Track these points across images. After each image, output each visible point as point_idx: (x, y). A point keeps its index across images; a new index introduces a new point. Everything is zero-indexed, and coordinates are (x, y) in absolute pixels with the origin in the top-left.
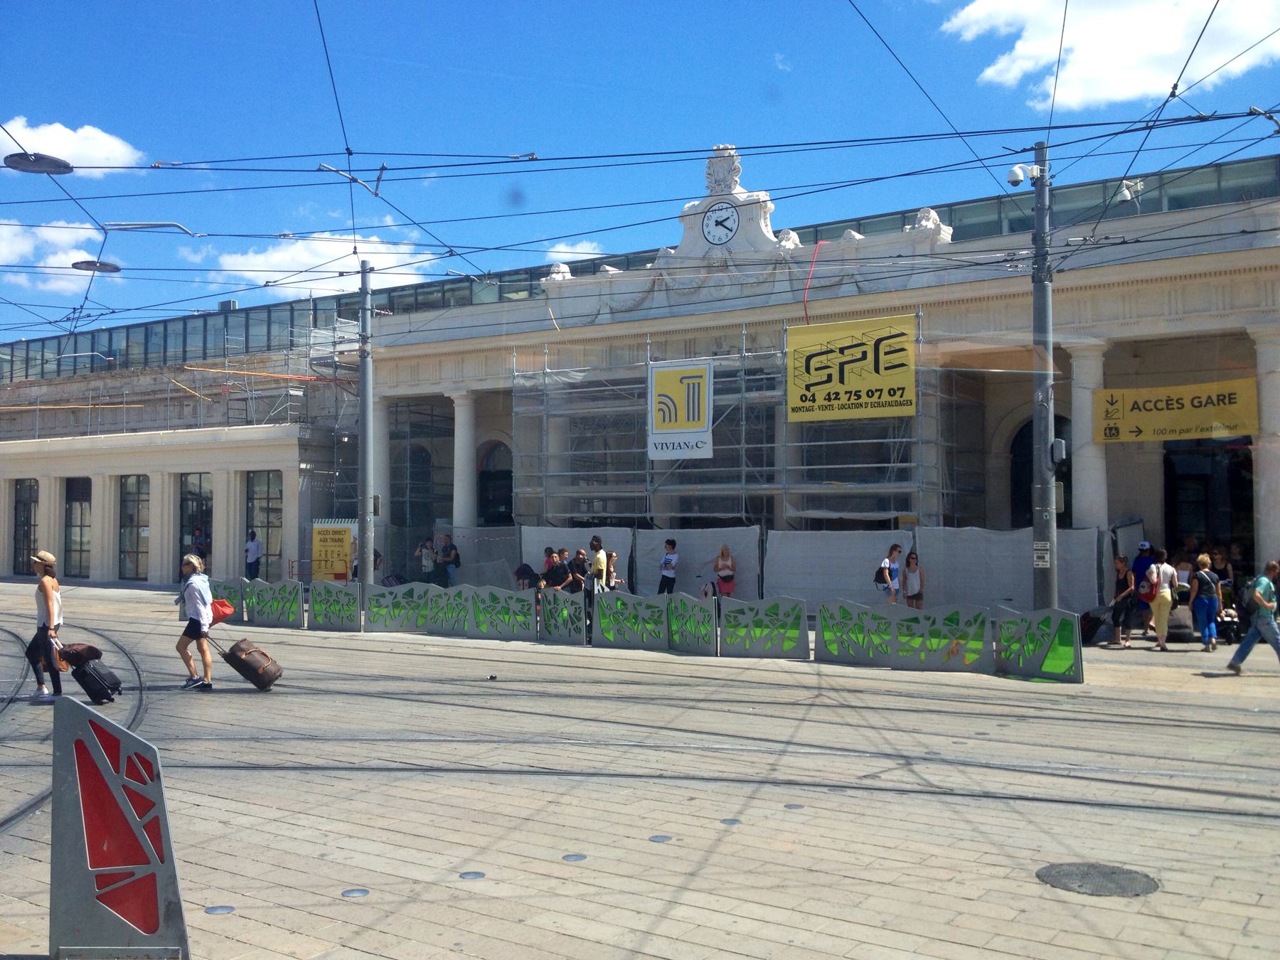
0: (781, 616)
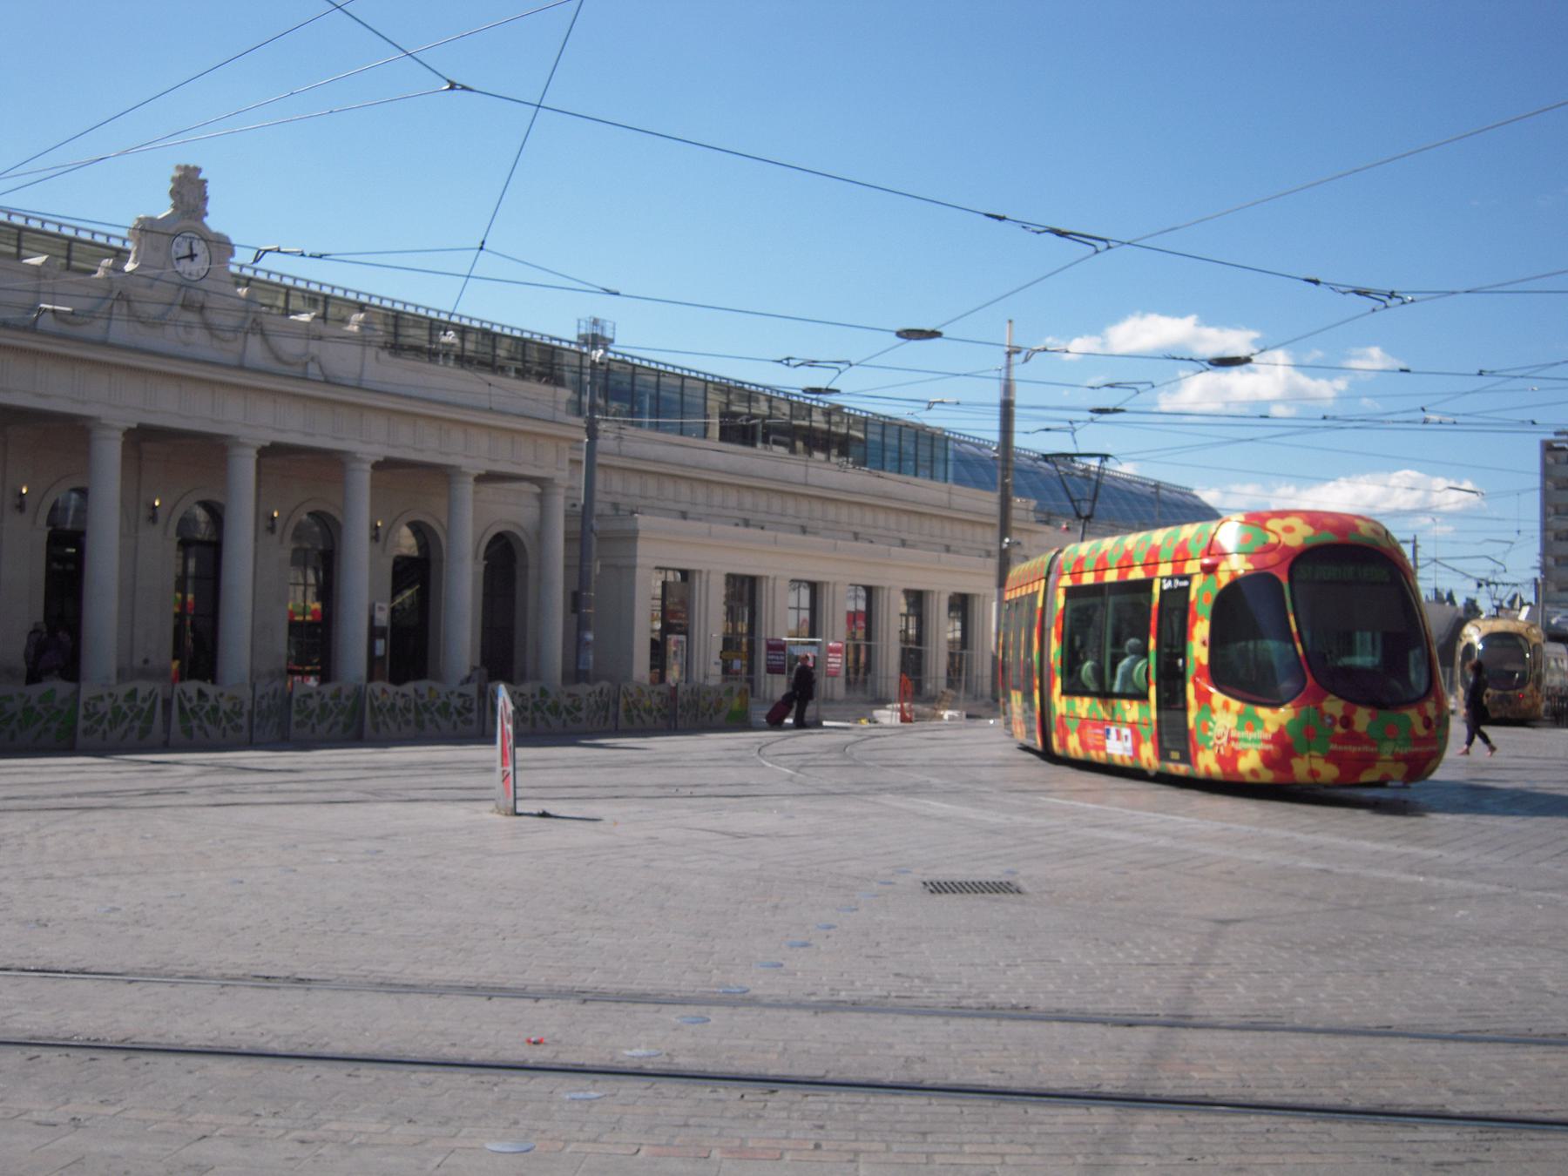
0: (139, 702)
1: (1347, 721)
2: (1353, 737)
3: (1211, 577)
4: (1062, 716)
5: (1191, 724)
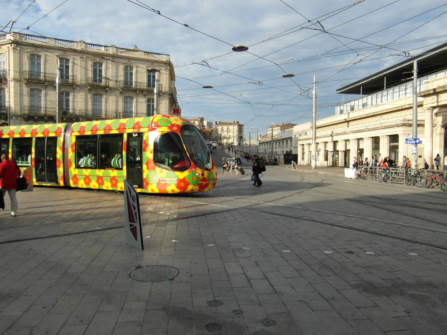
1: (203, 174)
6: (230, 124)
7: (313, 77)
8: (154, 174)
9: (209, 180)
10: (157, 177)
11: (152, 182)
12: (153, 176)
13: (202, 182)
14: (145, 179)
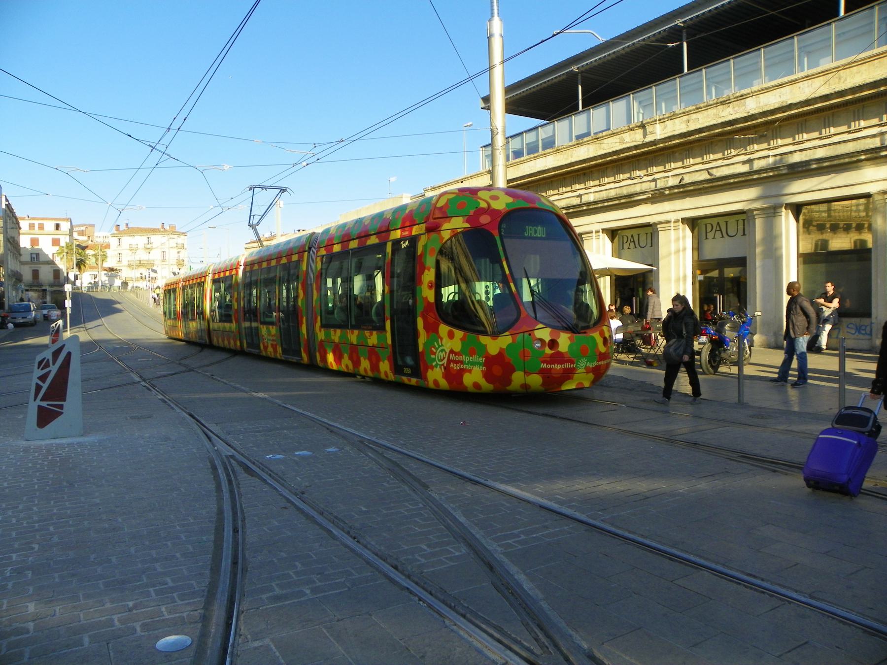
1: (553, 344)
2: (558, 357)
3: (434, 235)
4: (322, 341)
5: (421, 349)
6: (154, 231)
7: (578, 88)
8: (438, 344)
9: (575, 359)
10: (444, 352)
11: (434, 364)
12: (437, 349)
13: (549, 366)
14: (423, 352)
